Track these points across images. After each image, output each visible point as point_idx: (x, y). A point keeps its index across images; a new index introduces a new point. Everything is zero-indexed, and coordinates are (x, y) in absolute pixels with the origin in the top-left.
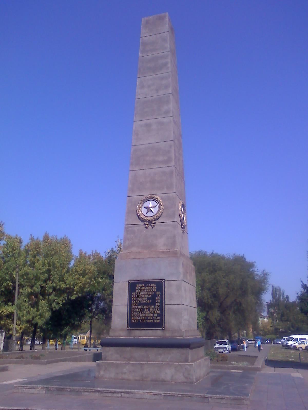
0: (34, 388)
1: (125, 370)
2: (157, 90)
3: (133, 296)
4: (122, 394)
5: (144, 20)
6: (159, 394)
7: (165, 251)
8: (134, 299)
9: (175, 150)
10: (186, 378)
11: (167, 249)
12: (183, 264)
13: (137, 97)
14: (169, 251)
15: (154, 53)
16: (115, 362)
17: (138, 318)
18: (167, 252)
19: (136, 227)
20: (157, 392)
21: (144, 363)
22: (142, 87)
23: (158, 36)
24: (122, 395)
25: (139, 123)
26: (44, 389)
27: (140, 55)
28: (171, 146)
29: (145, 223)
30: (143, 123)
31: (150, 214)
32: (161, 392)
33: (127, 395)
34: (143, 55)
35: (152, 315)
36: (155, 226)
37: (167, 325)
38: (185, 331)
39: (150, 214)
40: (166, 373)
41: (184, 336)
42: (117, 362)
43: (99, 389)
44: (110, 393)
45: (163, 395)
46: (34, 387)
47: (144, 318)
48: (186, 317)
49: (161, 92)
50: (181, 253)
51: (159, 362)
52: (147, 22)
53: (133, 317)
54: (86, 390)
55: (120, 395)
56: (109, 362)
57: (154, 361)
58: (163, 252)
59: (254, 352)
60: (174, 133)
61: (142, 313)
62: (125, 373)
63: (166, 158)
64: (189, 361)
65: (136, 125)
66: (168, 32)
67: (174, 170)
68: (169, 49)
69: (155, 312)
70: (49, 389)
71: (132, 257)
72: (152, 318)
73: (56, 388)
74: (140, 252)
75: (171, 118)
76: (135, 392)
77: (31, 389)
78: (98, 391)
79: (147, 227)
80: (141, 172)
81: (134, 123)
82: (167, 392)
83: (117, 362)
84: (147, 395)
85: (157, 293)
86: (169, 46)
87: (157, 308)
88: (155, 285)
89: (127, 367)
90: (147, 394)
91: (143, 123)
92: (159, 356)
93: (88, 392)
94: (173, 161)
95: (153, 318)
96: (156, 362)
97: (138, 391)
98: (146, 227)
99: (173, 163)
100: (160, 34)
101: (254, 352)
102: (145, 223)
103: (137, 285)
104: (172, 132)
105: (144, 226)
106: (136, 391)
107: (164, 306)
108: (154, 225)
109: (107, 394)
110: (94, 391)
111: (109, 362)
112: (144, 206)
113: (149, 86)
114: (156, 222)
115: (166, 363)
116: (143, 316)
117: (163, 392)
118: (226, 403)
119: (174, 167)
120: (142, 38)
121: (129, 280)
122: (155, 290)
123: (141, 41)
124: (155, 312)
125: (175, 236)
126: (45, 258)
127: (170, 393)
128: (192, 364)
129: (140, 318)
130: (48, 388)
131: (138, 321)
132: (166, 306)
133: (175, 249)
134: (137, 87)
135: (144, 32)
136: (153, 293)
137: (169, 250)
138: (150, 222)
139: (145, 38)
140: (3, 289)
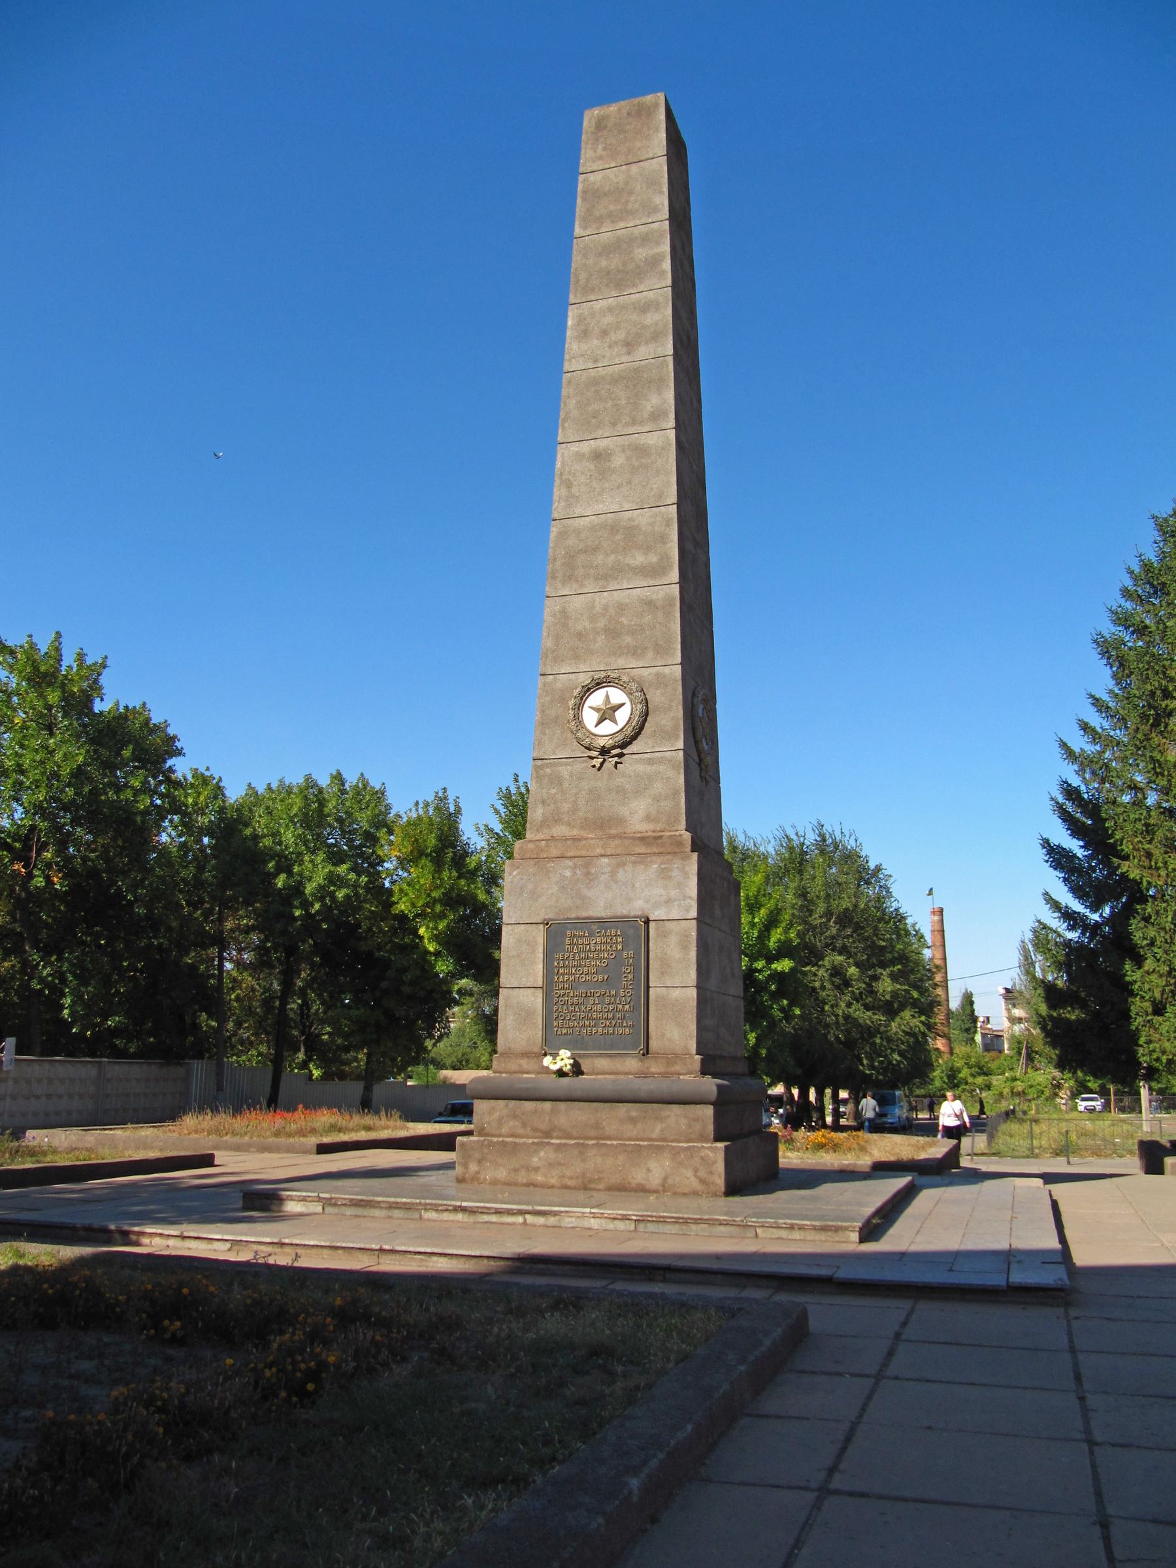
2: (629, 346)
4: (527, 1216)
5: (590, 117)
6: (624, 1218)
10: (702, 1181)
11: (654, 831)
13: (566, 367)
19: (567, 764)
20: (621, 1212)
22: (585, 334)
23: (634, 169)
24: (525, 1220)
25: (574, 448)
27: (578, 231)
30: (586, 447)
32: (630, 1213)
33: (541, 1220)
40: (649, 1170)
43: (464, 1204)
44: (492, 1213)
45: (636, 1220)
46: (291, 1196)
47: (587, 1023)
51: (630, 1139)
52: (600, 125)
55: (520, 1219)
58: (643, 839)
65: (564, 456)
70: (333, 1201)
71: (555, 852)
73: (351, 1200)
74: (576, 839)
78: (464, 1210)
80: (578, 602)
81: (570, 307)
82: (646, 1213)
84: (592, 1220)
89: (542, 1154)
91: (586, 447)
93: (437, 1210)
97: (568, 1209)
106: (562, 1209)
109: (486, 1218)
112: (590, 705)
113: (604, 333)
114: (625, 751)
115: (650, 1143)
117: (636, 1213)
118: (801, 1240)
120: (569, 374)
123: (580, 187)
124: (620, 1006)
127: (655, 1214)
130: (331, 1199)
133: (677, 831)
134: (569, 333)
135: (588, 156)
137: (660, 834)
139: (592, 177)
140: (744, 968)
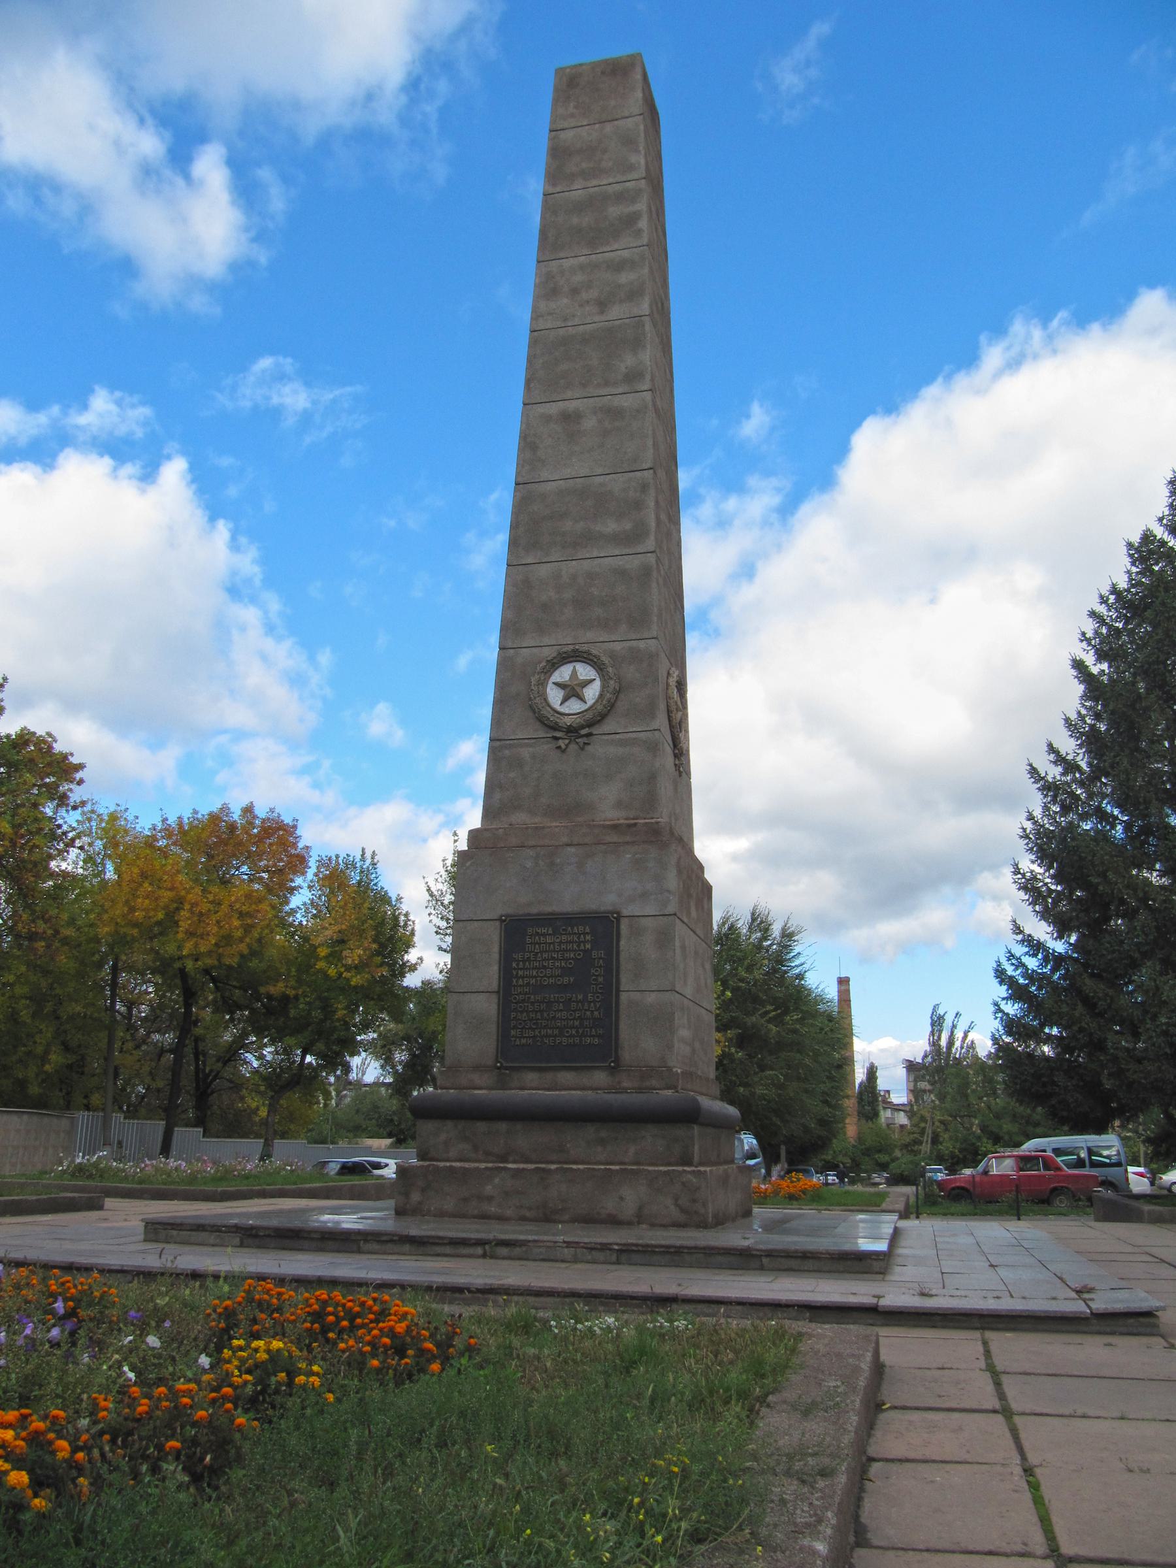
0: (206, 1231)
1: (488, 1189)
2: (602, 305)
3: (514, 965)
7: (620, 824)
8: (520, 973)
9: (657, 502)
10: (683, 1211)
11: (626, 819)
12: (678, 865)
14: (635, 824)
15: (595, 182)
16: (458, 1164)
17: (532, 1033)
18: (629, 826)
21: (553, 1167)
26: (236, 1232)
28: (644, 487)
29: (558, 734)
31: (574, 706)
34: (558, 190)
35: (577, 1023)
36: (589, 744)
37: (626, 1056)
38: (682, 1072)
39: (574, 706)
40: (621, 1198)
41: (680, 1087)
42: (467, 1165)
48: (684, 1033)
49: (616, 312)
50: (672, 833)
53: (515, 1027)
54: (369, 1238)
56: (442, 1164)
57: (583, 1163)
58: (615, 827)
59: (1024, 1298)
60: (654, 445)
61: (545, 1015)
62: (490, 1199)
63: (628, 526)
64: (696, 1159)
66: (642, 117)
67: (655, 566)
68: (642, 172)
69: (588, 1013)
72: (577, 1032)
75: (648, 396)
76: (529, 1241)
77: (194, 1233)
79: (563, 746)
83: (467, 1165)
85: (594, 954)
86: (643, 161)
87: (594, 1002)
88: (588, 930)
89: (497, 1181)
90: (567, 1247)
92: (600, 1149)
94: (652, 537)
95: (581, 1031)
96: (589, 1163)
98: (559, 747)
99: (650, 543)
100: (616, 122)
101: (1024, 1298)
102: (558, 734)
103: (530, 930)
104: (650, 443)
105: (553, 745)
107: (618, 996)
108: (585, 740)
110: (395, 1238)
111: (442, 1164)
114: (595, 730)
116: (546, 1027)
119: (653, 555)
121: (504, 913)
122: (588, 946)
125: (652, 777)
126: (106, 818)
128: (705, 1171)
129: (537, 1033)
131: (530, 1041)
132: (624, 997)
136: (570, 963)
138: (572, 731)
